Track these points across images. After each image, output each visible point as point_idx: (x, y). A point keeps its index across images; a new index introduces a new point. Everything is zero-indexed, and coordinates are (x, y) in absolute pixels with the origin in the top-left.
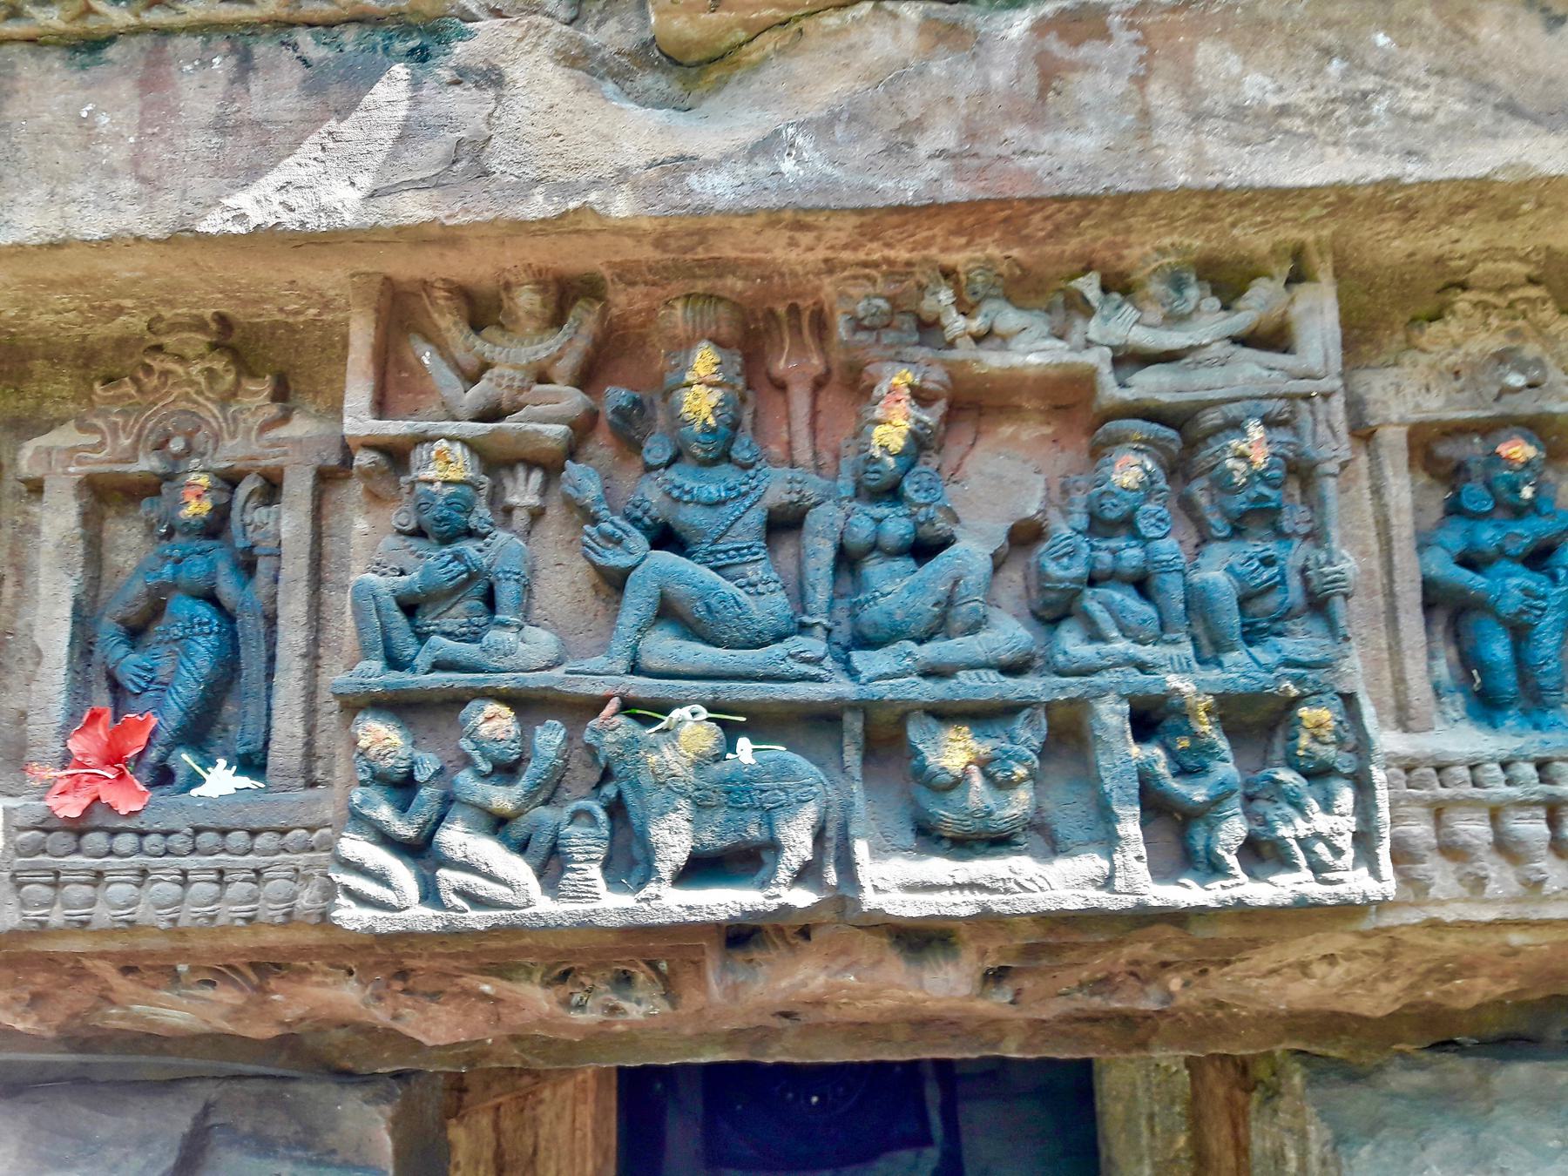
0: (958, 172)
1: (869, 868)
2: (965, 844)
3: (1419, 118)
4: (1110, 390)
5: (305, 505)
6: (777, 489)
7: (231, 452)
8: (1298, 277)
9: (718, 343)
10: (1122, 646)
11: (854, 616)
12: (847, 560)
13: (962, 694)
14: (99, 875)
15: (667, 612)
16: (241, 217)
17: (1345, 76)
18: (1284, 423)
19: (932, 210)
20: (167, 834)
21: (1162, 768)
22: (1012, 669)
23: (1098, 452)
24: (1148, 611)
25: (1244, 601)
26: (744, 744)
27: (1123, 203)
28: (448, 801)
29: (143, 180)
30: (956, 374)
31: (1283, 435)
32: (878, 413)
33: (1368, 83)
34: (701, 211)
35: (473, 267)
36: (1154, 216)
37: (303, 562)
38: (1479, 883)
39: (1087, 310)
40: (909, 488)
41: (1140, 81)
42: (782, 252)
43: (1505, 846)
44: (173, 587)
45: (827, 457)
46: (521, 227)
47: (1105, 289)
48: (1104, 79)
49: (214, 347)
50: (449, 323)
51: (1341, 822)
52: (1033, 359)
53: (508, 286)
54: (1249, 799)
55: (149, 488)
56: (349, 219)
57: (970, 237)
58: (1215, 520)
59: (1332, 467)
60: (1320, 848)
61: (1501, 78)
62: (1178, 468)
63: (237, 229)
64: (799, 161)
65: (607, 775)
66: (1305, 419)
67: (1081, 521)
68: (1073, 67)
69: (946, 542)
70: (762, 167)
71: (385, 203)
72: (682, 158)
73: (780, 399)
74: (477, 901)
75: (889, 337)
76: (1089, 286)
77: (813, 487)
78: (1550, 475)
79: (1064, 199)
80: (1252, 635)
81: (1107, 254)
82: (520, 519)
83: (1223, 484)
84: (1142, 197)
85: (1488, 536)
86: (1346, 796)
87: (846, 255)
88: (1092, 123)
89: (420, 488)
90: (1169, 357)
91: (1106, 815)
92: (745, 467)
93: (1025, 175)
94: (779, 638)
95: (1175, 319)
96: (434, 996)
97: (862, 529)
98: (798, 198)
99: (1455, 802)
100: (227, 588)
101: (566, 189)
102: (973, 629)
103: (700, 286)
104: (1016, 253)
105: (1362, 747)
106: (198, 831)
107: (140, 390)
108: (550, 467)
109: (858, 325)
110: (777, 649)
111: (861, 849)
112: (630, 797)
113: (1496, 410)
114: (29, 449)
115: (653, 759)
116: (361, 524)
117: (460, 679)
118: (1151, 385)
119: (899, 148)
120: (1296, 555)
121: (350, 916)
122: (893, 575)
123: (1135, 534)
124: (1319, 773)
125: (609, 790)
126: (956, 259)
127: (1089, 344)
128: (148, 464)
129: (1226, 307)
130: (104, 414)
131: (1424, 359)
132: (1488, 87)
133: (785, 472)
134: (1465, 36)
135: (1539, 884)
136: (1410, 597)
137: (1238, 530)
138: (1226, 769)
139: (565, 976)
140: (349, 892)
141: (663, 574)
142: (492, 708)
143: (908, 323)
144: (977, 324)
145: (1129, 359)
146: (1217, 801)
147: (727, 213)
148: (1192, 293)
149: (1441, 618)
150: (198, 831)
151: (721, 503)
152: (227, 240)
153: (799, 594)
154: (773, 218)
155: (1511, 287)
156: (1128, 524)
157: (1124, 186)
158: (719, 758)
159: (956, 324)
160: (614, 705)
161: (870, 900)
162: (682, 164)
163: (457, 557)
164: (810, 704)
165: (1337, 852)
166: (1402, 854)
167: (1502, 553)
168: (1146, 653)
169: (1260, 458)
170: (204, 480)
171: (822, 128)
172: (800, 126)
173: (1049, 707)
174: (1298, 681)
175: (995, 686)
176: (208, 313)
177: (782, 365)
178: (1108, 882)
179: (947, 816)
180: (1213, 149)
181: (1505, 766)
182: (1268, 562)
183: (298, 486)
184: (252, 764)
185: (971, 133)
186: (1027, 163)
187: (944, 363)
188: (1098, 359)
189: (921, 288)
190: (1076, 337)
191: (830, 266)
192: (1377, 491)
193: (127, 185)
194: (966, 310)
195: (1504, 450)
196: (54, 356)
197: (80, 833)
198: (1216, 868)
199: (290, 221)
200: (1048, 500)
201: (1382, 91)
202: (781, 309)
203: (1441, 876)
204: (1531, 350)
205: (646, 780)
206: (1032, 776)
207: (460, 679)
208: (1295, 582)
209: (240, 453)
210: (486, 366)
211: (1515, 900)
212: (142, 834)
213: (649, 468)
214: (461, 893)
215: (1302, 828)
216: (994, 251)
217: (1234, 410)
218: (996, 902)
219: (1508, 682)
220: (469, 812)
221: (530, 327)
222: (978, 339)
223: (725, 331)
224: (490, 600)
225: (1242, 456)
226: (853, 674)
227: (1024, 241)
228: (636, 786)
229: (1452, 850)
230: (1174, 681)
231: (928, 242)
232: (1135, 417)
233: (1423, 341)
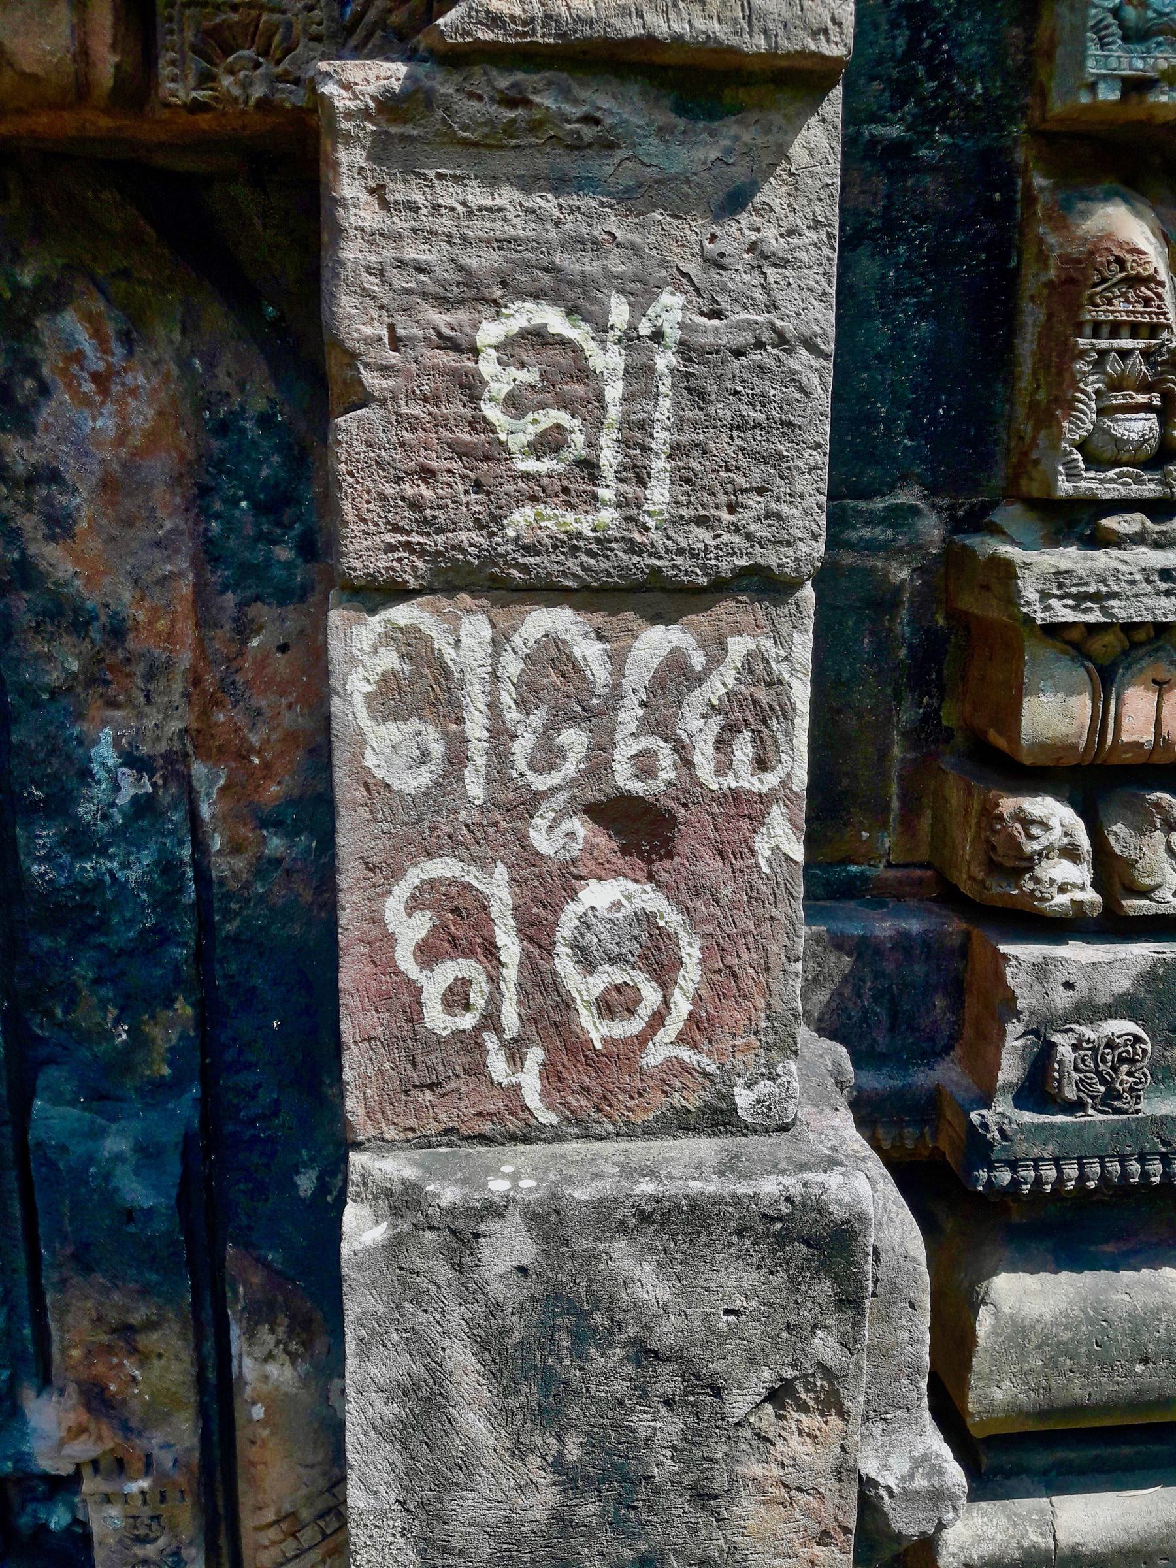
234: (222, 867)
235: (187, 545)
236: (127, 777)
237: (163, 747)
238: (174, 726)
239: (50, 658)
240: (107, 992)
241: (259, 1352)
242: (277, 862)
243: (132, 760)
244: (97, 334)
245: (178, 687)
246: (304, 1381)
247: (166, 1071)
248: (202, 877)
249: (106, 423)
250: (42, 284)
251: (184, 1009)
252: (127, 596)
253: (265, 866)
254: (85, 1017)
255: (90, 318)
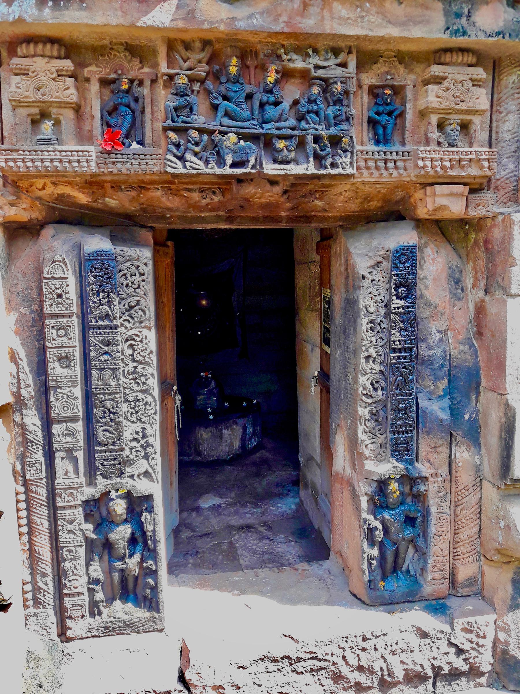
0: (287, 26)
1: (265, 166)
2: (282, 163)
3: (373, 22)
4: (313, 73)
5: (149, 88)
6: (248, 89)
7: (132, 74)
8: (350, 52)
9: (237, 57)
10: (312, 125)
11: (262, 117)
12: (262, 105)
13: (283, 133)
14: (114, 163)
15: (227, 114)
16: (145, 23)
17: (360, 12)
18: (345, 83)
19: (282, 33)
20: (127, 155)
21: (318, 148)
22: (293, 129)
23: (310, 86)
24: (318, 119)
25: (335, 118)
26: (242, 141)
27: (317, 35)
28: (187, 149)
29: (123, 12)
30: (284, 67)
31: (344, 85)
32: (269, 74)
33: (364, 14)
34: (238, 30)
35: (187, 37)
36: (323, 38)
37: (150, 100)
38: (372, 174)
39: (309, 56)
40: (274, 91)
41: (322, 9)
42: (251, 38)
43: (377, 168)
44: (121, 104)
45: (257, 83)
46: (202, 30)
47: (313, 52)
48: (316, 8)
49: (125, 49)
50: (181, 48)
51: (348, 160)
52: (299, 66)
53: (193, 41)
54: (333, 156)
55: (114, 81)
56: (168, 25)
57: (288, 39)
58: (331, 102)
59: (352, 92)
60: (344, 164)
61: (388, 15)
62: (325, 90)
63: (144, 25)
64: (257, 21)
65: (216, 146)
66: (348, 83)
67: (306, 100)
68: (310, 5)
69: (281, 102)
70: (250, 21)
71: (175, 22)
72: (233, 18)
73: (247, 70)
74: (194, 168)
75: (271, 58)
76: (310, 51)
77: (255, 89)
78: (394, 98)
79: (307, 33)
80: (336, 125)
81: (314, 45)
82: (195, 92)
83: (333, 94)
84: (321, 34)
85: (381, 109)
86: (349, 155)
87: (263, 40)
88: (313, 18)
89: (177, 85)
90: (324, 67)
91: (308, 157)
92: (242, 84)
93: (300, 28)
94: (248, 121)
95: (326, 60)
96: (176, 195)
97: (265, 99)
98: (257, 29)
99: (369, 159)
100: (133, 104)
101: (211, 23)
102: (286, 120)
103: (233, 44)
104: (296, 43)
105: (353, 147)
106: (134, 154)
107: (110, 59)
108: (202, 82)
109: (265, 55)
110: (248, 123)
111: (264, 163)
112: (221, 150)
113: (385, 83)
114: (86, 70)
115: (225, 143)
116: (163, 92)
117: (188, 125)
118: (321, 73)
119: (276, 20)
120: (344, 109)
121: (170, 170)
122: (271, 109)
123: (316, 103)
124: (345, 151)
125: (217, 149)
126: (285, 43)
127: (310, 63)
128: (113, 76)
129: (336, 58)
130: (102, 64)
131: (373, 71)
132: (386, 17)
133: (249, 86)
134: (382, 4)
135: (382, 174)
136: (366, 120)
137: (335, 104)
138: (329, 149)
139: (202, 191)
140: (169, 166)
141: (226, 105)
142: (194, 131)
143: (275, 56)
144: (289, 57)
145: (317, 67)
146: (327, 155)
147: (244, 30)
148: (330, 54)
149: (371, 125)
150: (134, 154)
151: (237, 91)
152: (142, 27)
153: (252, 113)
154: (251, 32)
155: (391, 57)
156: (315, 101)
157: (318, 32)
158: (237, 144)
159: (284, 57)
160: (217, 132)
161: (265, 171)
162: (234, 19)
163: (185, 100)
164: (255, 133)
165: (347, 165)
166: (358, 168)
167: (383, 112)
168: (316, 127)
169: (340, 89)
170: (126, 80)
171: (262, 13)
172: (257, 13)
173: (299, 136)
174: (343, 133)
175: (289, 132)
176: (123, 41)
177: (249, 63)
178: (307, 169)
179: (279, 156)
180: (335, 25)
181: (378, 153)
182: (339, 110)
183: (147, 83)
184: (141, 143)
185: (290, 18)
186: (300, 25)
187: (282, 65)
188: (311, 67)
189: (278, 48)
190: (307, 62)
191: (260, 42)
192: (362, 99)
193: (120, 13)
194: (286, 54)
195: (386, 92)
196: (86, 48)
197: (109, 154)
198: (326, 168)
199: (155, 25)
200: (300, 96)
201: (366, 16)
202: (248, 50)
203: (365, 173)
204: (393, 71)
205: (224, 147)
206: (295, 150)
207: (188, 125)
208: (344, 115)
209: (134, 75)
210: (188, 59)
211: (377, 178)
212: (122, 155)
213: (221, 83)
214: (190, 167)
215: (341, 161)
216: (292, 42)
217: (336, 79)
218: (288, 172)
219: (381, 138)
220: (191, 151)
221: (198, 51)
222: (289, 60)
223: (238, 54)
224: (191, 110)
225: (336, 89)
226: (262, 128)
227: (298, 40)
228: (222, 148)
229: (368, 168)
230: (321, 132)
231: (280, 39)
232: (53, 496)
233: (373, 68)
234: (453, 352)
235: (448, 290)
236: (438, 334)
237: (444, 329)
238: (445, 324)
239: (425, 312)
240: (431, 377)
241: (462, 451)
242: (462, 351)
243: (439, 332)
244: (433, 252)
245: (446, 317)
246: (470, 457)
247: (442, 393)
248: (450, 355)
249: (434, 268)
250: (425, 243)
251: (446, 381)
252: (438, 300)
253: (460, 352)
254: (426, 383)
255: (432, 249)
